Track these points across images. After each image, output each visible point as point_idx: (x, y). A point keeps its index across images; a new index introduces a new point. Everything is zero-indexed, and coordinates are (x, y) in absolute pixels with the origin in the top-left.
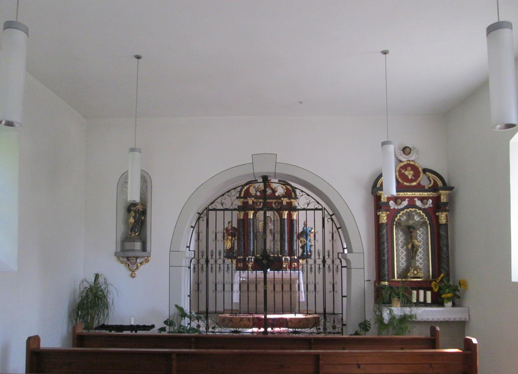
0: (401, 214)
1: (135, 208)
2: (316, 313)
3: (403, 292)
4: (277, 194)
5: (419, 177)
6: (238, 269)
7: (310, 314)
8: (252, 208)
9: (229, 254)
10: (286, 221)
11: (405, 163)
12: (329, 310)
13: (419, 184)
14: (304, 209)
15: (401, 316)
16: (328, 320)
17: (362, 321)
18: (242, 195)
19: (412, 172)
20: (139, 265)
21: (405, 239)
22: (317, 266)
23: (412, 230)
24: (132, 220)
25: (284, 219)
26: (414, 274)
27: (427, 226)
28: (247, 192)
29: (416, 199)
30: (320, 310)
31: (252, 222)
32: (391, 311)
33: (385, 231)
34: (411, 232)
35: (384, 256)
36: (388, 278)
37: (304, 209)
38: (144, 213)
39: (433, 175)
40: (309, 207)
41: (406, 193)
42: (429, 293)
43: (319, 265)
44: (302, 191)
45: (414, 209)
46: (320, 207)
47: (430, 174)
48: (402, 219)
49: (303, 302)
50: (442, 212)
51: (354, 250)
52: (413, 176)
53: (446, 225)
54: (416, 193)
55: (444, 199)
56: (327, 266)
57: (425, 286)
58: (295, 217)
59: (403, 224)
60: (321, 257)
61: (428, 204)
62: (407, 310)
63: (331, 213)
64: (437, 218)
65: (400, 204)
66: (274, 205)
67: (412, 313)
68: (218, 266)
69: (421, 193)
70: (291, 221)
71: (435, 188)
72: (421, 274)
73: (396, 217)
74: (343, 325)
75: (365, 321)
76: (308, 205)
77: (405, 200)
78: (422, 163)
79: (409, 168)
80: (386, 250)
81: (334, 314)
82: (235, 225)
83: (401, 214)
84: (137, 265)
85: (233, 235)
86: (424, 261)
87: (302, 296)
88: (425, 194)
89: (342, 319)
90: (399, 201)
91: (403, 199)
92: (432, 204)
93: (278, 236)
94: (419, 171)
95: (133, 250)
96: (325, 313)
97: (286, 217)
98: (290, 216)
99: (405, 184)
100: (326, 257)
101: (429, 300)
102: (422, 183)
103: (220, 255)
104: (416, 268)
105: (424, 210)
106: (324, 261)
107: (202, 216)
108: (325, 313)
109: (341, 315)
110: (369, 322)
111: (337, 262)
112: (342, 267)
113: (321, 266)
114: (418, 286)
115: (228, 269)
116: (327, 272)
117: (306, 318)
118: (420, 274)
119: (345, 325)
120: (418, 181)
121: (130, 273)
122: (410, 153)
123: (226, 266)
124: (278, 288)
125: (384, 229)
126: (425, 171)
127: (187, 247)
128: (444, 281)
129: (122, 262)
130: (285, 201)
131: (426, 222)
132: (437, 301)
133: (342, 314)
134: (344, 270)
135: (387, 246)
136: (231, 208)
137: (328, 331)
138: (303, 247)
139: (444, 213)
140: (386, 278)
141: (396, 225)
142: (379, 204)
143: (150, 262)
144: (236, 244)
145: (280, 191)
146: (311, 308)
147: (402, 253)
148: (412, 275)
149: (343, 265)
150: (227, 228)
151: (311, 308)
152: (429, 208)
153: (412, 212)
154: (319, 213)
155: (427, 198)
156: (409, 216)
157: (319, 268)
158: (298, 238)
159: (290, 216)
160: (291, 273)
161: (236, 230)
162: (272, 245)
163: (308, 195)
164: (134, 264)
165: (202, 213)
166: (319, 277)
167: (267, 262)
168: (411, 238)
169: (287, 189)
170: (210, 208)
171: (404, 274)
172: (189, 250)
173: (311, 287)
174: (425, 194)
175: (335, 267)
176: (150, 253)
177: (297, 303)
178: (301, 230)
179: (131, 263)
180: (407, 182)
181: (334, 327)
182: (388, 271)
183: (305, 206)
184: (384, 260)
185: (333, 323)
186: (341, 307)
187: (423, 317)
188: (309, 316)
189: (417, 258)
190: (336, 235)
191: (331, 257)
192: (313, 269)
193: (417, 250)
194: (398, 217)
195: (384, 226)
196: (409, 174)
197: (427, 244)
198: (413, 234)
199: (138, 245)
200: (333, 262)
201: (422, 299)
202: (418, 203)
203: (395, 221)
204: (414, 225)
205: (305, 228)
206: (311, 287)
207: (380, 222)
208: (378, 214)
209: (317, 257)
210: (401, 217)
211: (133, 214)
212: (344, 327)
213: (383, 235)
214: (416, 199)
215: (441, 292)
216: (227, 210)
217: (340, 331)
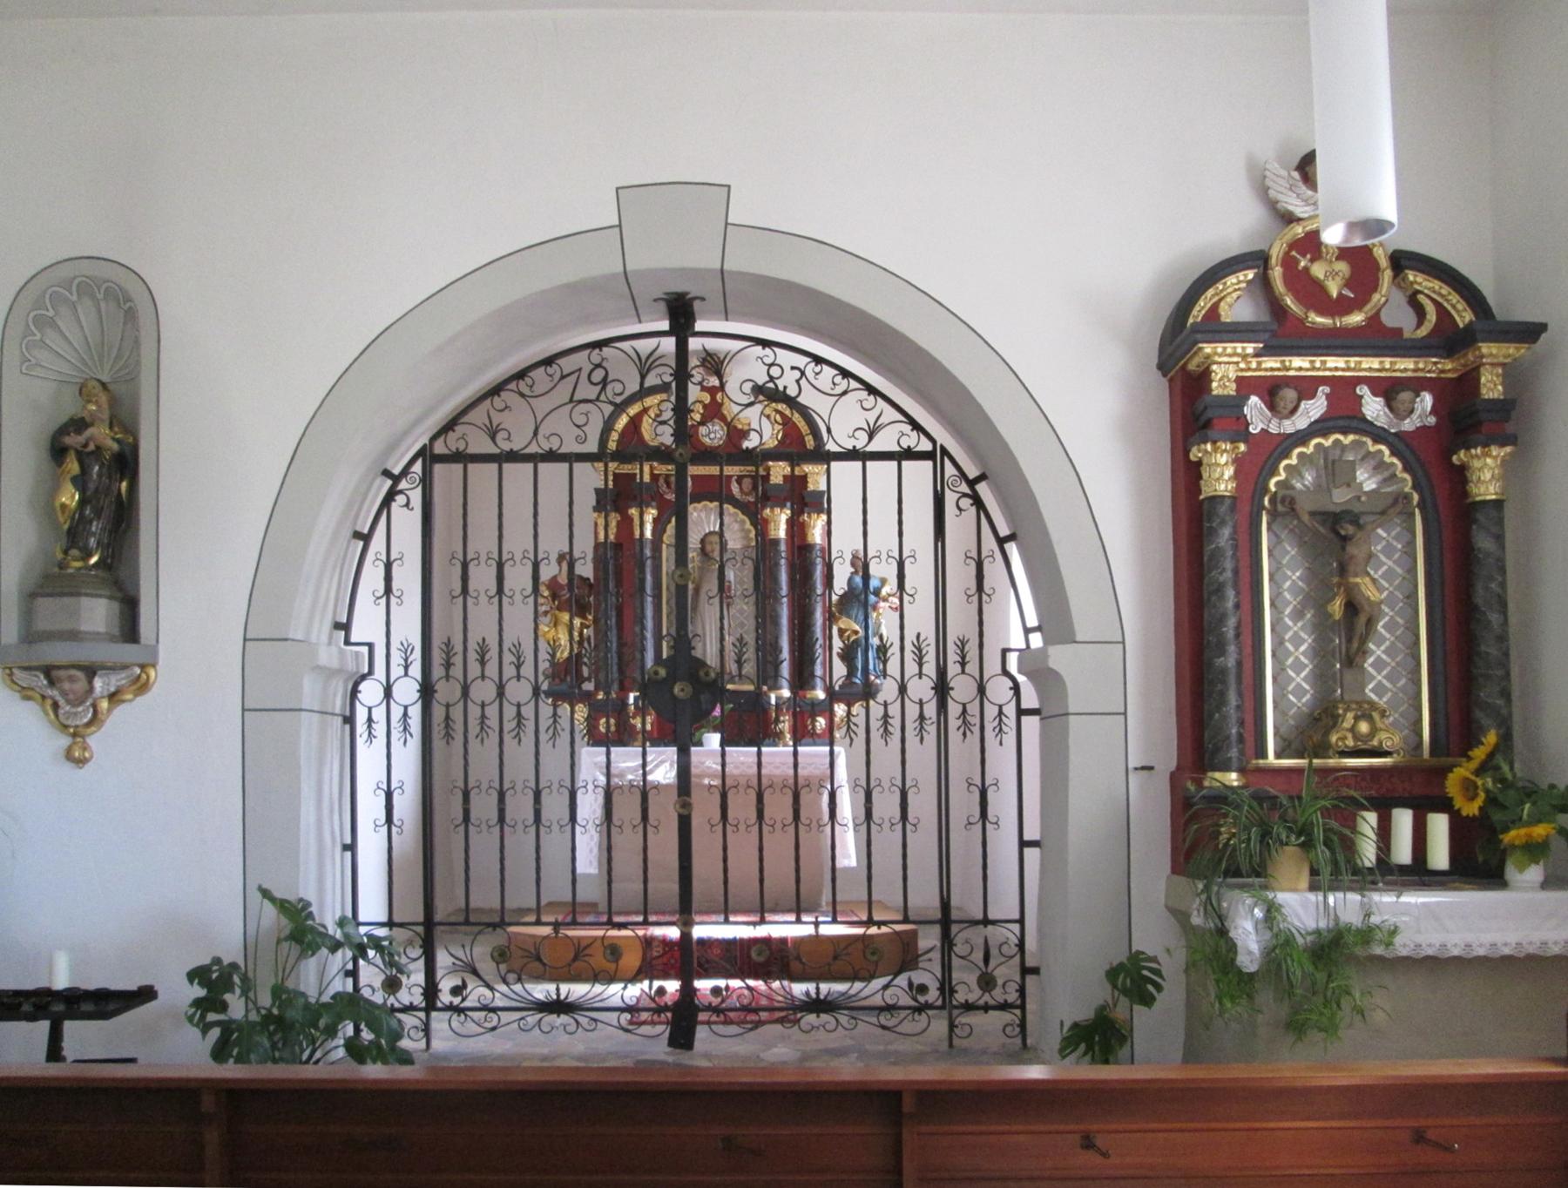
0: (1294, 461)
1: (81, 439)
2: (906, 920)
3: (1315, 819)
5: (1375, 287)
6: (596, 739)
7: (880, 924)
10: (783, 547)
12: (966, 902)
13: (1374, 320)
14: (852, 455)
15: (1318, 932)
16: (959, 949)
17: (1121, 957)
20: (104, 704)
21: (1312, 575)
22: (912, 711)
23: (1348, 529)
24: (69, 497)
25: (776, 542)
27: (1413, 514)
29: (1363, 390)
30: (925, 898)
32: (1272, 910)
33: (1226, 532)
34: (1345, 539)
35: (1221, 650)
36: (1242, 752)
37: (852, 455)
38: (126, 463)
39: (1436, 284)
40: (875, 446)
41: (1318, 361)
42: (1439, 824)
43: (921, 703)
44: (845, 374)
45: (1351, 437)
46: (926, 446)
49: (847, 870)
50: (1486, 445)
51: (1083, 627)
52: (1348, 284)
53: (1498, 504)
55: (1491, 387)
56: (954, 710)
57: (1418, 788)
58: (816, 535)
59: (1305, 506)
60: (930, 668)
61: (1415, 416)
62: (1347, 905)
63: (972, 473)
64: (1460, 476)
65: (1294, 411)
66: (735, 489)
67: (1375, 919)
68: (474, 712)
69: (1387, 362)
70: (801, 548)
71: (1449, 340)
72: (1386, 739)
73: (1274, 471)
74: (1026, 971)
75: (1136, 958)
76: (871, 437)
77: (1312, 396)
80: (1232, 622)
81: (986, 922)
82: (586, 570)
83: (1294, 461)
84: (94, 706)
87: (844, 846)
88: (1405, 366)
89: (1021, 945)
90: (1289, 394)
91: (1306, 387)
92: (1434, 411)
95: (73, 636)
96: (946, 920)
98: (797, 529)
100: (953, 669)
101: (1439, 856)
102: (1389, 319)
103: (483, 662)
104: (1366, 711)
105: (1399, 443)
106: (942, 689)
107: (403, 485)
108: (946, 920)
109: (1016, 928)
110: (1154, 959)
111: (999, 690)
112: (1021, 712)
113: (931, 710)
114: (1383, 793)
115: (519, 724)
116: (954, 736)
117: (864, 936)
118: (1383, 735)
119: (1035, 971)
120: (1369, 308)
121: (65, 741)
123: (510, 712)
124: (741, 807)
125: (1223, 523)
126: (1401, 261)
127: (338, 626)
128: (1497, 768)
129: (26, 693)
130: (779, 471)
132: (1478, 862)
133: (1021, 921)
134: (1031, 724)
135: (1237, 606)
136: (533, 449)
137: (960, 997)
138: (848, 656)
139: (1495, 450)
140: (1234, 753)
141: (1274, 515)
142: (1193, 410)
143: (155, 690)
145: (763, 431)
146: (888, 890)
147: (1297, 641)
148: (1350, 742)
149: (1024, 706)
150: (554, 578)
151: (888, 890)
152: (1423, 429)
153: (1344, 448)
154: (919, 474)
155: (1416, 385)
156: (1334, 470)
157: (922, 717)
159: (797, 529)
160: (795, 754)
161: (591, 586)
162: (720, 633)
163: (872, 390)
164: (82, 702)
165: (405, 472)
166: (923, 757)
167: (689, 689)
168: (1343, 570)
169: (787, 422)
170: (439, 448)
171: (1312, 733)
172: (347, 642)
173: (887, 806)
174: (1405, 366)
175: (991, 712)
176: (154, 651)
177: (828, 876)
178: (840, 585)
179: (64, 694)
180: (1321, 313)
181: (987, 982)
182: (1242, 723)
183: (860, 442)
184: (1224, 671)
185: (981, 964)
186: (1007, 884)
187: (1420, 939)
188: (873, 930)
189: (1368, 663)
190: (994, 569)
191: (972, 668)
192: (896, 722)
193: (1371, 623)
194: (1282, 476)
195: (1223, 509)
197: (1412, 597)
198: (1352, 549)
199: (97, 613)
200: (981, 690)
201: (1403, 852)
202: (1373, 407)
203: (1266, 490)
205: (858, 580)
206: (887, 806)
207: (1207, 491)
208: (1195, 454)
209: (911, 668)
210: (1294, 473)
211: (73, 466)
212: (1030, 979)
213: (1217, 554)
214: (1363, 390)
215: (1497, 816)
216: (514, 457)
217: (1013, 997)
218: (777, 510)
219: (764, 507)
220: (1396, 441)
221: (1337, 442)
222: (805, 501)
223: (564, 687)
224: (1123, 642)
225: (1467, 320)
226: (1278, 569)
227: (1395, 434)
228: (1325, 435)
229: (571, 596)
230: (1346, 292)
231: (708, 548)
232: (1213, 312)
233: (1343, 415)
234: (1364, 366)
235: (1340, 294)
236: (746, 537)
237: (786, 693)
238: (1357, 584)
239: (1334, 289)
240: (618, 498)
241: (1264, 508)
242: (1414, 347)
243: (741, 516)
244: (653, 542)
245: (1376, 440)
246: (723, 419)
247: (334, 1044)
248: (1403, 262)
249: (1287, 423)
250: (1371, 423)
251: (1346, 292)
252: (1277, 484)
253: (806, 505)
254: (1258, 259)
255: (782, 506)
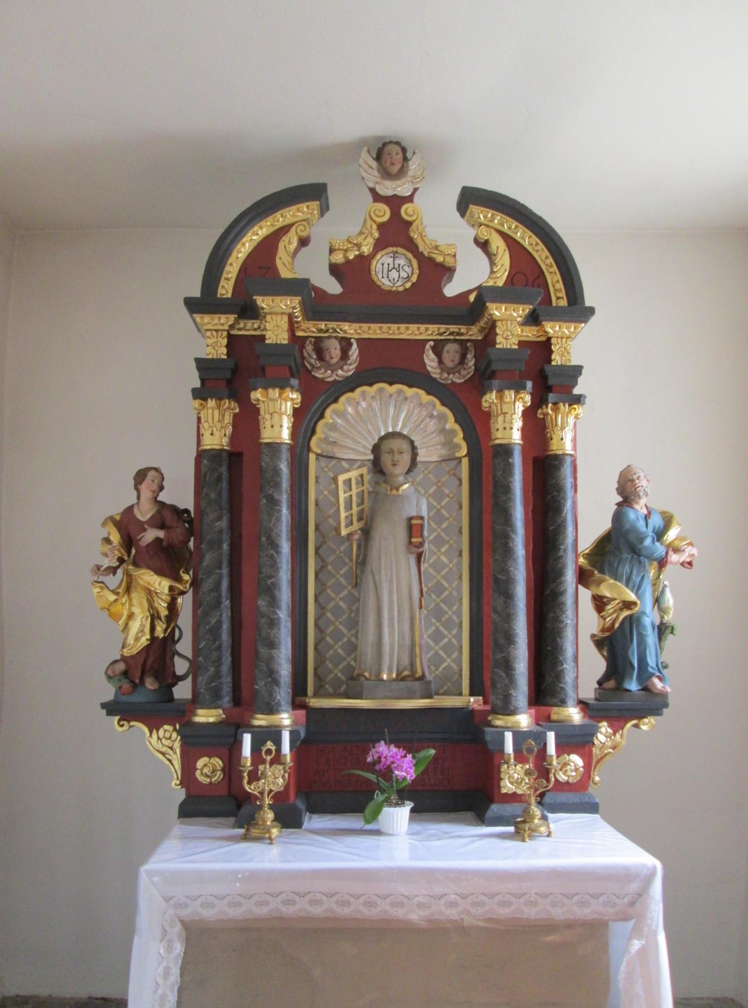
4: (451, 290)
8: (287, 363)
9: (145, 686)
10: (517, 460)
18: (226, 289)
25: (505, 451)
28: (261, 271)
31: (284, 468)
66: (430, 361)
82: (181, 493)
85: (168, 559)
93: (451, 561)
97: (516, 436)
98: (537, 428)
144: (185, 620)
158: (583, 577)
159: (537, 428)
218: (509, 395)
219: (483, 391)
222: (549, 382)
223: (138, 698)
226: (324, 543)
229: (158, 542)
231: (386, 459)
236: (449, 444)
237: (524, 720)
240: (231, 377)
243: (441, 408)
244: (292, 448)
246: (411, 246)
247: (337, 379)
253: (549, 389)
255: (519, 388)
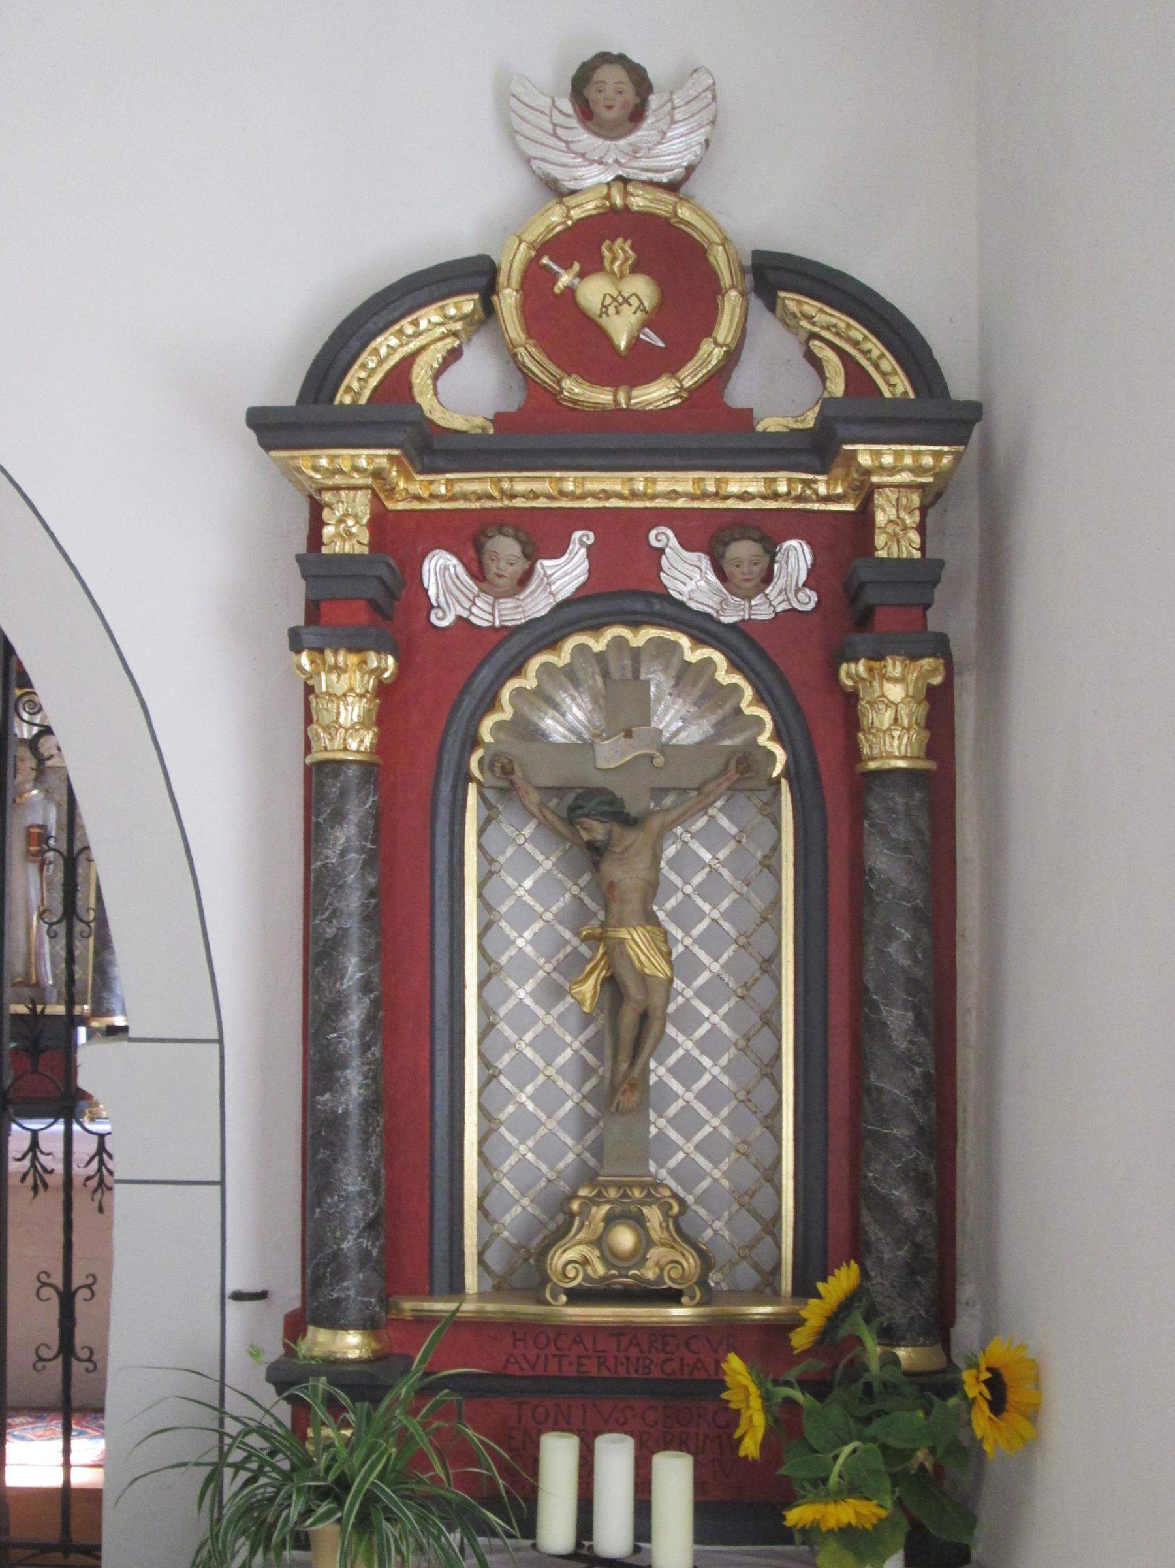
11: (589, 206)
19: (642, 288)
26: (610, 1256)
29: (661, 537)
42: (674, 1475)
47: (811, 306)
48: (554, 728)
52: (651, 321)
54: (664, 481)
64: (849, 709)
65: (524, 580)
77: (559, 550)
78: (745, 213)
79: (619, 252)
83: (529, 681)
86: (724, 1117)
88: (744, 487)
90: (505, 550)
92: (813, 580)
94: (712, 276)
99: (574, 388)
105: (740, 642)
122: (637, 115)
126: (773, 275)
131: (748, 763)
139: (894, 667)
155: (768, 530)
194: (506, 713)
196: (619, 301)
202: (688, 577)
204: (619, 788)
214: (661, 537)
220: (734, 639)
221: (619, 641)
224: (220, 1041)
225: (900, 389)
227: (732, 626)
228: (596, 628)
230: (651, 338)
232: (398, 381)
233: (625, 591)
234: (734, 488)
235: (636, 343)
238: (622, 941)
239: (622, 329)
241: (469, 778)
242: (773, 451)
245: (552, 643)
248: (771, 275)
249: (507, 604)
250: (682, 604)
251: (651, 338)
252: (499, 726)
254: (476, 276)
